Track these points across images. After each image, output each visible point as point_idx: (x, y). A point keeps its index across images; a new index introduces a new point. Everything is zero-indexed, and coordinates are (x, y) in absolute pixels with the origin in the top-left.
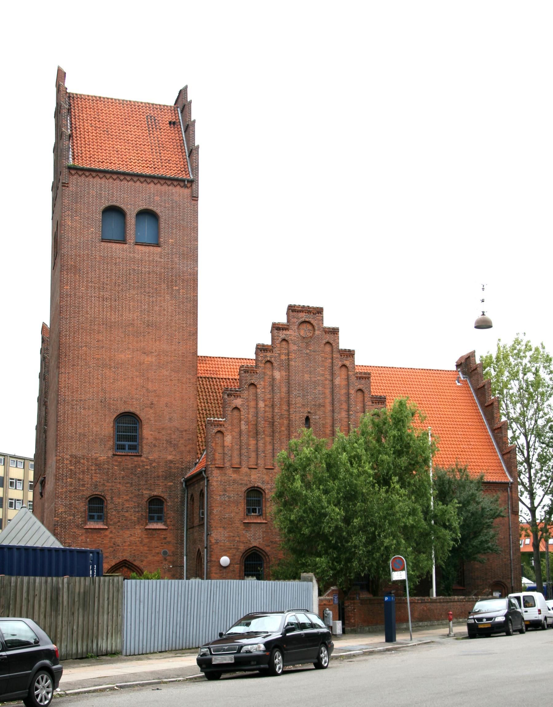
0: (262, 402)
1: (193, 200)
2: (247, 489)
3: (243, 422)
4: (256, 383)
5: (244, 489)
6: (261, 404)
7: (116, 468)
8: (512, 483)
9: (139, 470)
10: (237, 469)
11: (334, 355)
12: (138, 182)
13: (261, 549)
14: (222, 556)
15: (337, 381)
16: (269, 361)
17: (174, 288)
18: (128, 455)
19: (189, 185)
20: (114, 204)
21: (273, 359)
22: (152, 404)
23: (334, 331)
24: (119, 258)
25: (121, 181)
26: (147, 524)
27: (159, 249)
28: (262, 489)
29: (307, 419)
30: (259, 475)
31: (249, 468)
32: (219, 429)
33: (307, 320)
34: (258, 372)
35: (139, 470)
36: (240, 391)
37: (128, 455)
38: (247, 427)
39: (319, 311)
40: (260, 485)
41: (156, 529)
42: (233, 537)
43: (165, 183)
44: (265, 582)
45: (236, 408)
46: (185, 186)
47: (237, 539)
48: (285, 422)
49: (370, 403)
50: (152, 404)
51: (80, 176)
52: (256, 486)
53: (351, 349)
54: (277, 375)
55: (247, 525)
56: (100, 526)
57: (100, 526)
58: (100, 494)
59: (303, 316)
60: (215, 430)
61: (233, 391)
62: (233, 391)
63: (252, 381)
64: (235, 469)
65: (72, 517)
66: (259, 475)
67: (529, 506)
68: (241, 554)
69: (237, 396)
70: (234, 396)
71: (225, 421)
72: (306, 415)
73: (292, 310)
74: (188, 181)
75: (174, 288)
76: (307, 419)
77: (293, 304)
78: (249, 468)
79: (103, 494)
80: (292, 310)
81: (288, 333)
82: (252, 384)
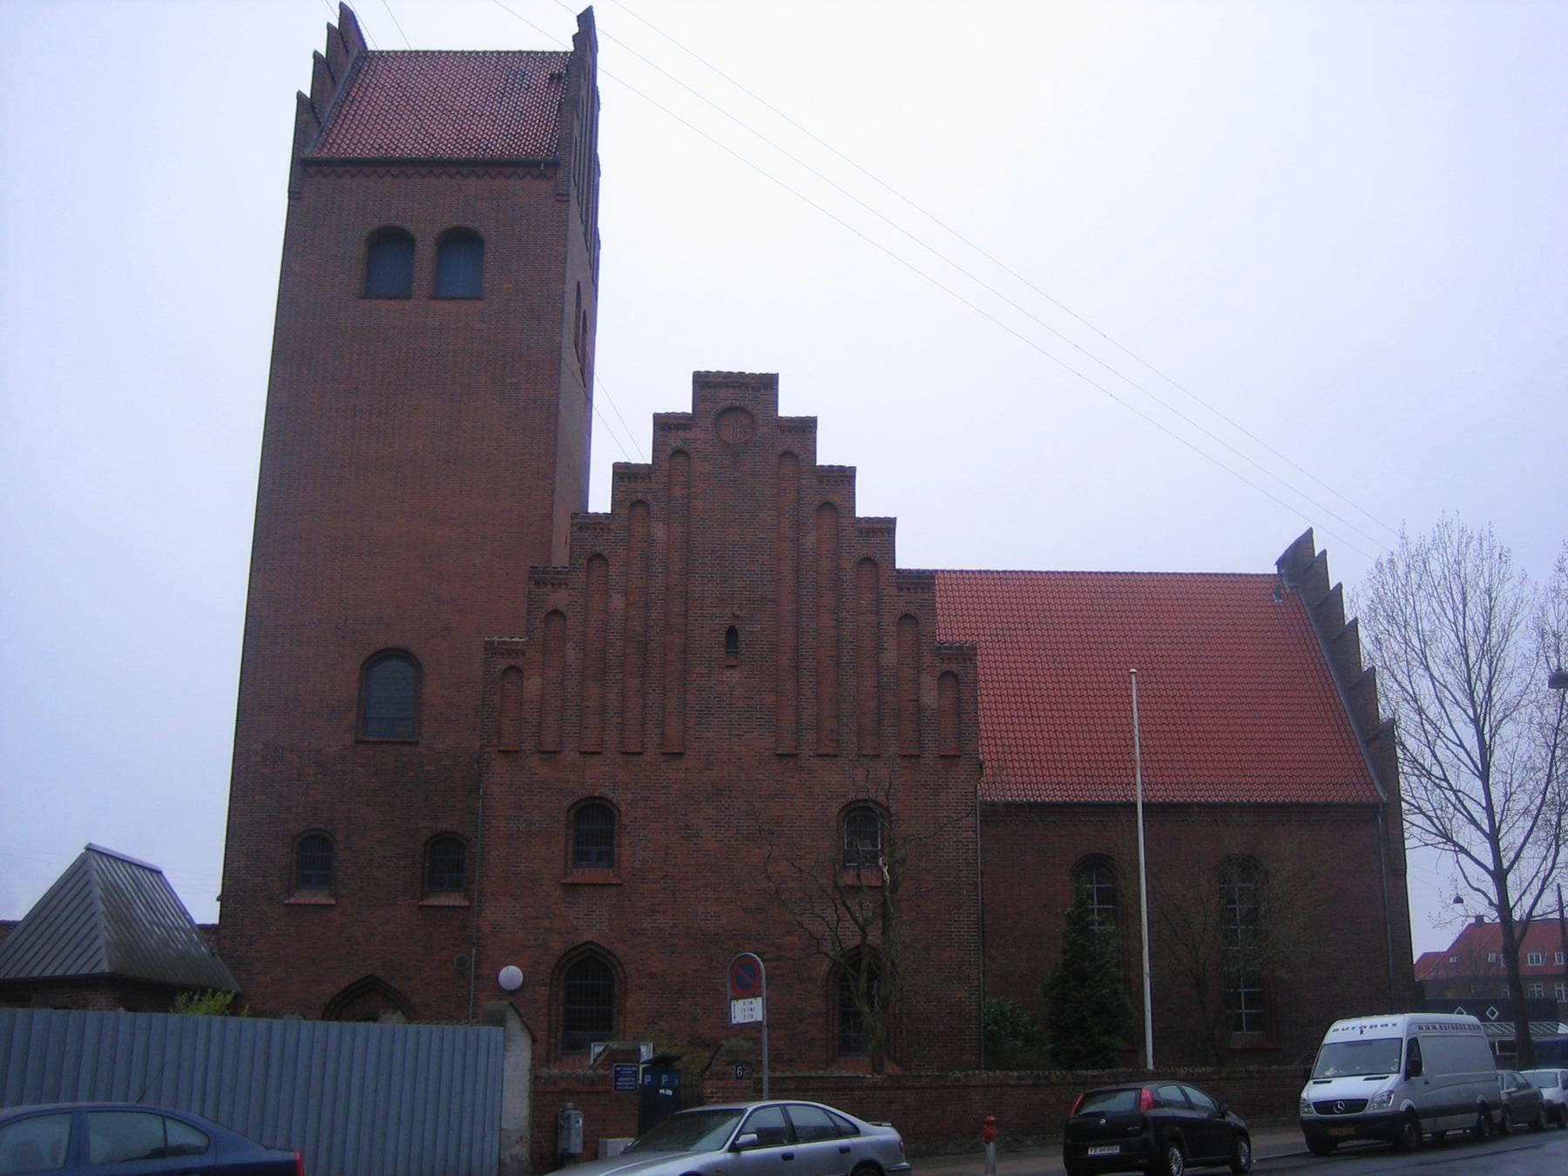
0: (619, 596)
1: (558, 201)
2: (577, 803)
3: (570, 645)
4: (606, 553)
5: (567, 803)
6: (618, 602)
7: (360, 769)
8: (1385, 805)
9: (411, 773)
10: (550, 755)
11: (804, 482)
12: (444, 177)
13: (605, 949)
14: (500, 970)
15: (809, 542)
16: (639, 502)
17: (508, 381)
18: (388, 743)
19: (550, 173)
20: (393, 222)
21: (650, 496)
22: (447, 629)
23: (807, 427)
24: (394, 328)
25: (409, 177)
26: (424, 896)
27: (480, 304)
28: (611, 802)
29: (732, 633)
30: (607, 768)
31: (582, 753)
32: (512, 662)
33: (737, 403)
34: (612, 527)
35: (411, 773)
36: (567, 573)
37: (388, 743)
38: (580, 656)
39: (767, 384)
40: (606, 792)
41: (443, 907)
42: (537, 918)
43: (501, 173)
44: (436, 1029)
45: (555, 613)
46: (542, 176)
47: (546, 923)
48: (677, 641)
49: (894, 591)
50: (447, 629)
51: (326, 176)
52: (596, 794)
53: (847, 464)
54: (659, 532)
55: (570, 889)
56: (322, 898)
57: (322, 898)
58: (324, 827)
59: (728, 397)
60: (503, 664)
61: (549, 572)
62: (549, 572)
63: (598, 549)
64: (547, 756)
65: (259, 880)
66: (607, 768)
67: (1492, 868)
68: (555, 961)
69: (557, 585)
70: (553, 584)
71: (525, 644)
72: (728, 622)
73: (705, 383)
74: (547, 165)
75: (508, 381)
76: (732, 633)
77: (703, 369)
78: (582, 753)
79: (329, 828)
80: (705, 383)
81: (690, 435)
82: (598, 556)
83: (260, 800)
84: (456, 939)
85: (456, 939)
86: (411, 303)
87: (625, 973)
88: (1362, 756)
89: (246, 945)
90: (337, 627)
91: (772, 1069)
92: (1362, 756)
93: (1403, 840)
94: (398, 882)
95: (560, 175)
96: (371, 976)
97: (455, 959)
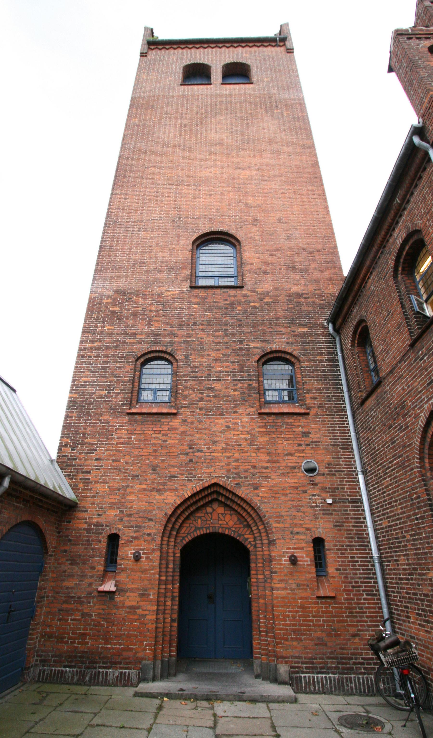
50: (256, 220)
65: (104, 393)
79: (169, 350)
83: (108, 329)
84: (300, 445)
85: (300, 445)
86: (212, 86)
87: (162, 540)
88: (201, 439)
89: (86, 453)
90: (173, 221)
91: (345, 677)
92: (201, 439)
93: (204, 534)
94: (236, 393)
95: (287, 43)
96: (216, 485)
97: (303, 465)
